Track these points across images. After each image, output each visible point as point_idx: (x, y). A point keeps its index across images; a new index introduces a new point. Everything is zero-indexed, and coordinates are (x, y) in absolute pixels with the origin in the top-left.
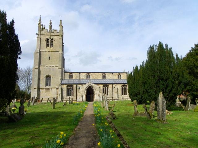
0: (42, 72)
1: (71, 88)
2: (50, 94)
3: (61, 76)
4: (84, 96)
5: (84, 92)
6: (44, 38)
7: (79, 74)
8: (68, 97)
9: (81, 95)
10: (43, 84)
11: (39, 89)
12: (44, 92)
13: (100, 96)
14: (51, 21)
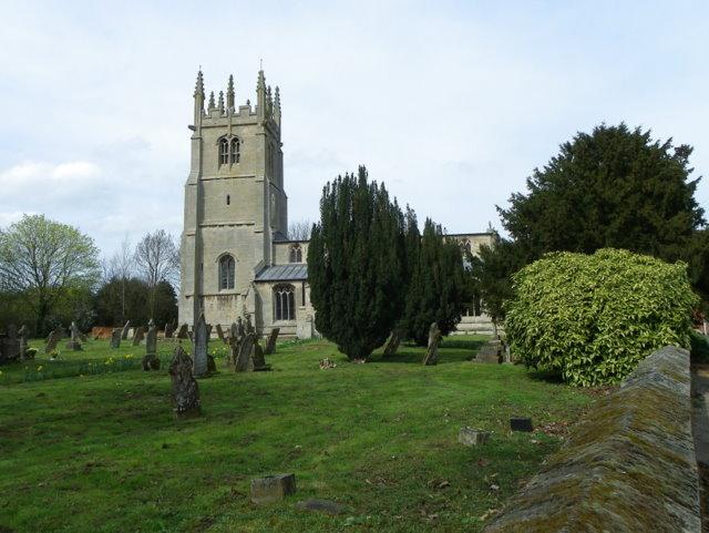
0: (207, 246)
3: (262, 255)
6: (211, 137)
10: (211, 284)
11: (199, 298)
12: (215, 306)
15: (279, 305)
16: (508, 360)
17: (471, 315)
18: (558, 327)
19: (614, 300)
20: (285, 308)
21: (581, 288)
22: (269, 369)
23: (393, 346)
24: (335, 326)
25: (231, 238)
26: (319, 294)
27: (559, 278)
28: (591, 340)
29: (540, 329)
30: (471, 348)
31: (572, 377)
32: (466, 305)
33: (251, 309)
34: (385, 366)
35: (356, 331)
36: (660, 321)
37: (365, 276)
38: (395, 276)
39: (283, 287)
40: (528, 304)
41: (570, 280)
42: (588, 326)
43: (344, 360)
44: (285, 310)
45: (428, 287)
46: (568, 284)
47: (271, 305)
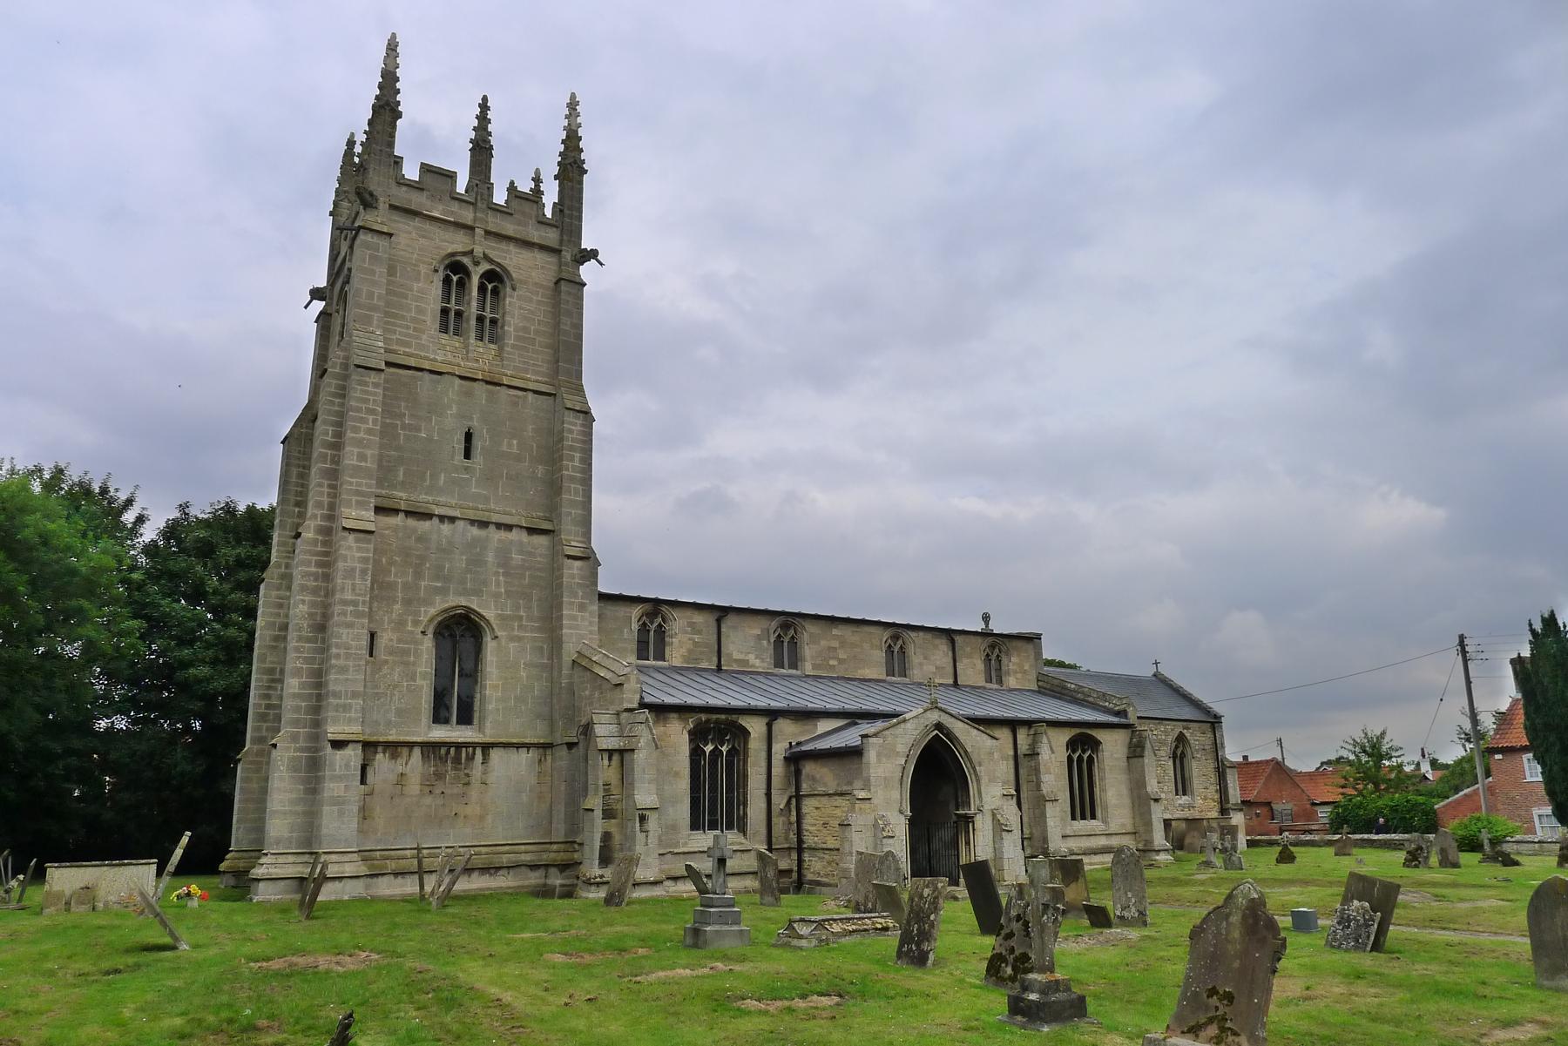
1: (724, 749)
2: (469, 810)
4: (899, 826)
5: (896, 795)
7: (719, 621)
8: (704, 840)
12: (414, 786)
14: (484, 106)
25: (477, 562)
44: (713, 811)
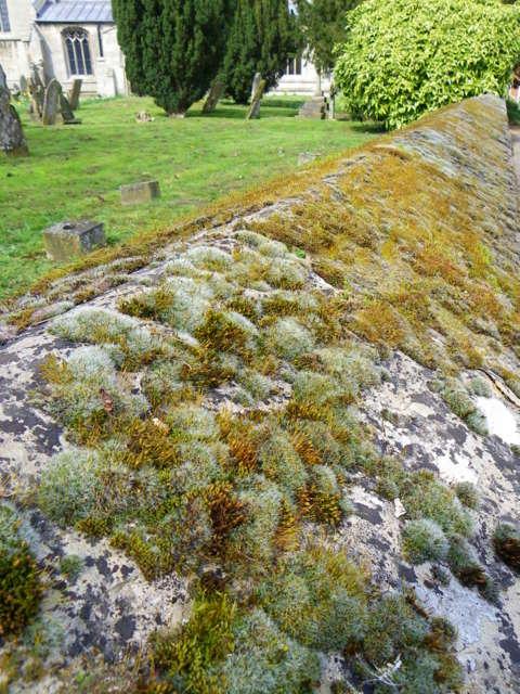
9: (110, 70)
13: (114, 76)
15: (71, 57)
16: (331, 117)
17: (291, 72)
18: (389, 72)
19: (447, 43)
20: (80, 59)
21: (418, 29)
22: (80, 123)
23: (212, 102)
24: (150, 74)
26: (128, 33)
27: (396, 17)
28: (417, 88)
29: (371, 75)
30: (292, 107)
31: (395, 126)
32: (290, 55)
33: (38, 58)
34: (207, 120)
35: (173, 79)
36: (485, 68)
37: (181, 11)
38: (217, 13)
39: (73, 30)
40: (360, 47)
41: (406, 20)
42: (418, 72)
43: (160, 115)
44: (80, 63)
45: (249, 34)
46: (405, 23)
47: (63, 65)
